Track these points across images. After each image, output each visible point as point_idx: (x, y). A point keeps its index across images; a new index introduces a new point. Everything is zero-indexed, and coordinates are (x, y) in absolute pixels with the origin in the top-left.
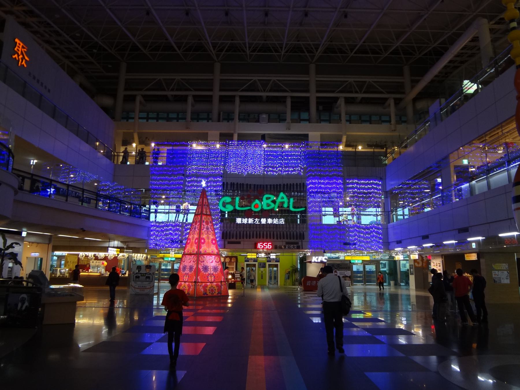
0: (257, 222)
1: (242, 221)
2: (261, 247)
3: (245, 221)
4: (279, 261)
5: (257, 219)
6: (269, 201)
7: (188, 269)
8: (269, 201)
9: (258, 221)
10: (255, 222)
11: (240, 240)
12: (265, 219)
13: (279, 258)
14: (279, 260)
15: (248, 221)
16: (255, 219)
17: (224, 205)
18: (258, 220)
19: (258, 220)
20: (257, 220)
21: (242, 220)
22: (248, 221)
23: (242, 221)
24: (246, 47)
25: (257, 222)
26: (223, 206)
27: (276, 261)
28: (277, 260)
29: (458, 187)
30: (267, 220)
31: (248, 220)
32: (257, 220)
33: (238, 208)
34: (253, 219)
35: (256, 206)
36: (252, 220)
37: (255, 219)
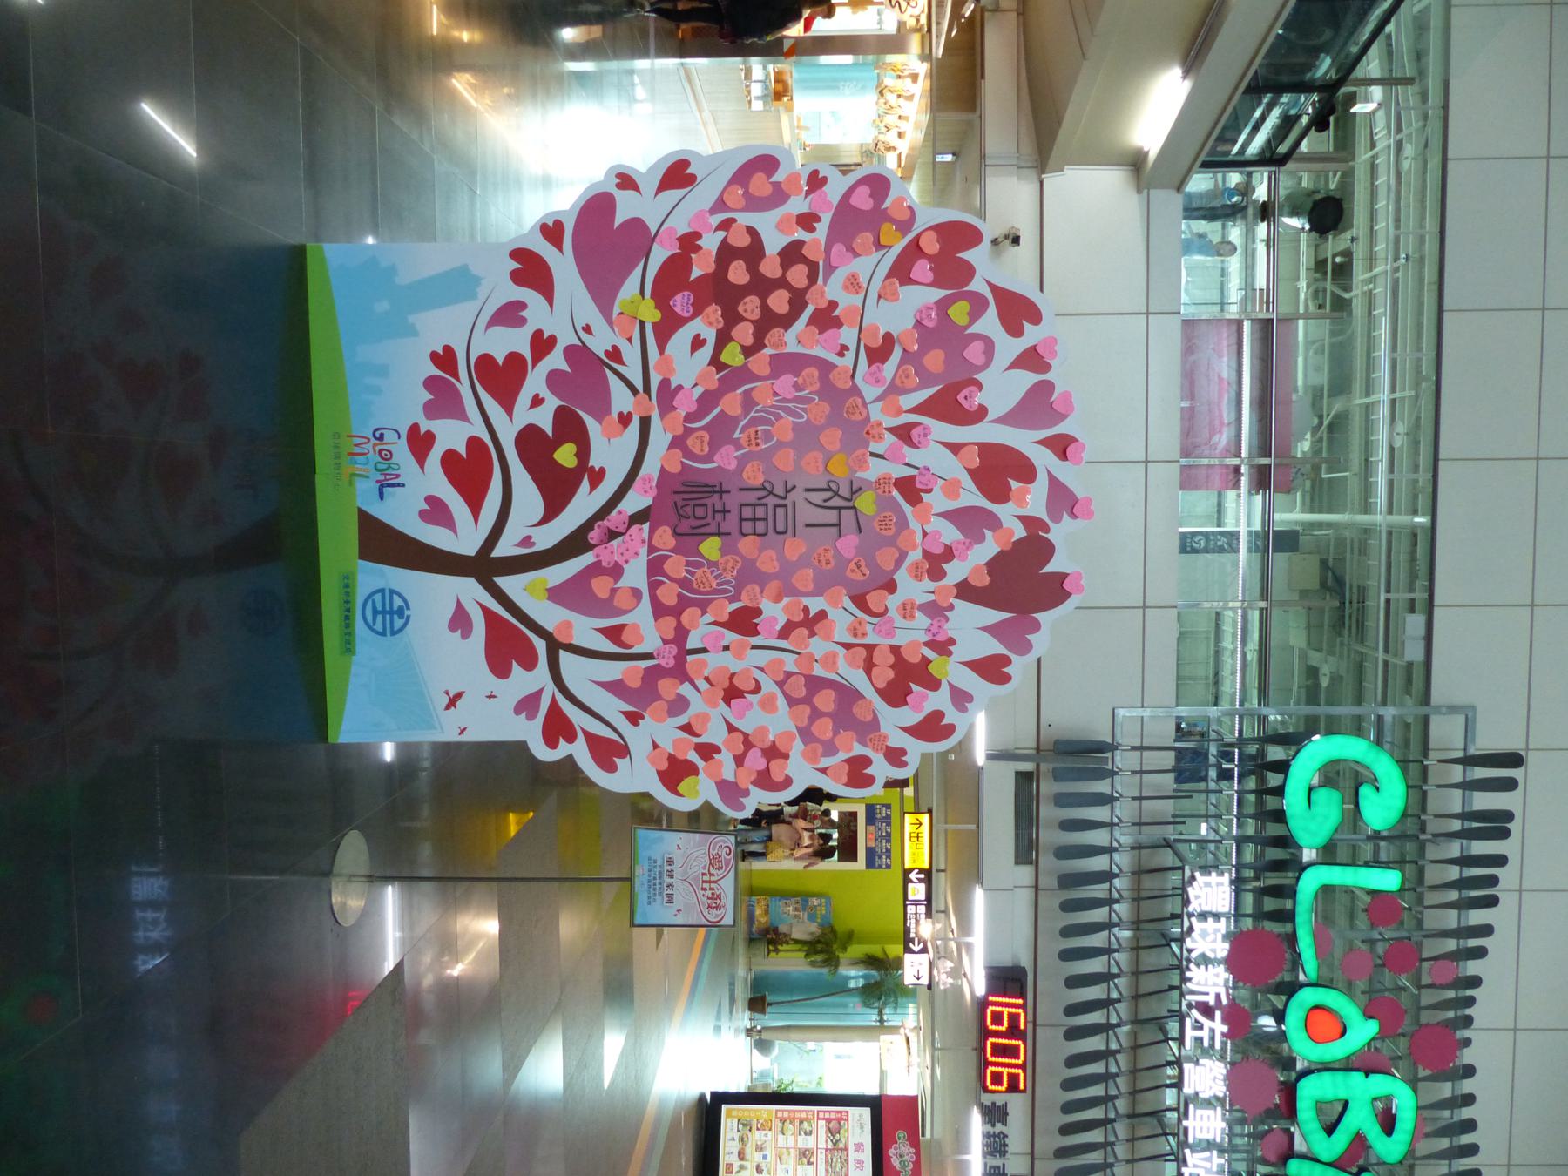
0: (1198, 1033)
1: (1203, 916)
2: (997, 1078)
3: (1209, 940)
4: (870, 864)
5: (1225, 1029)
6: (1360, 1119)
7: (879, 816)
8: (1360, 1119)
9: (1205, 1034)
10: (1195, 1013)
11: (1047, 861)
12: (1220, 1089)
13: (888, 867)
14: (880, 867)
15: (1205, 960)
16: (1218, 1014)
17: (1338, 776)
18: (1212, 1039)
19: (1212, 1039)
20: (1212, 1031)
21: (1217, 916)
22: (1205, 960)
23: (1203, 916)
24: (1328, 415)
25: (1198, 1033)
26: (1337, 762)
27: (870, 853)
28: (880, 857)
29: (902, 494)
30: (1208, 1103)
31: (1216, 962)
32: (1212, 1031)
33: (1310, 883)
34: (1225, 1001)
35: (1324, 1024)
36: (1213, 991)
37: (1218, 1014)
